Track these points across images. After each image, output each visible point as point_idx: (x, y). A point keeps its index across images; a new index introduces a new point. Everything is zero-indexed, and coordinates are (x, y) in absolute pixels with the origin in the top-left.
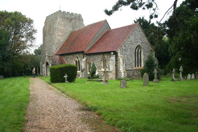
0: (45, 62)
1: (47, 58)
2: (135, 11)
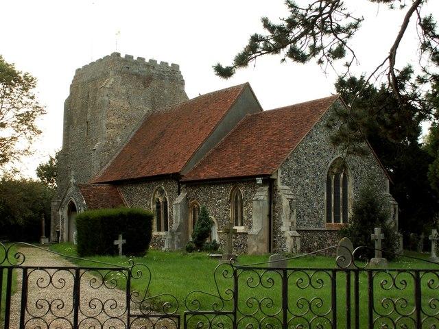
0: (66, 202)
1: (71, 190)
2: (300, 64)
